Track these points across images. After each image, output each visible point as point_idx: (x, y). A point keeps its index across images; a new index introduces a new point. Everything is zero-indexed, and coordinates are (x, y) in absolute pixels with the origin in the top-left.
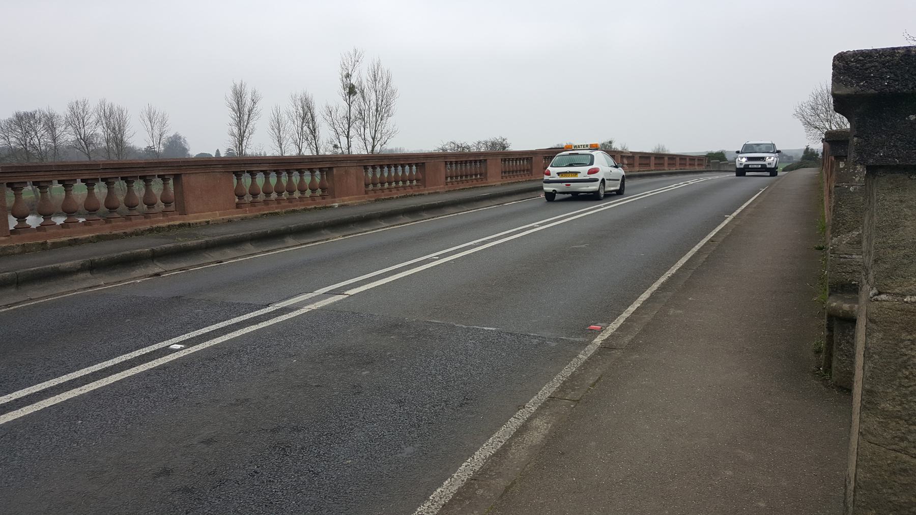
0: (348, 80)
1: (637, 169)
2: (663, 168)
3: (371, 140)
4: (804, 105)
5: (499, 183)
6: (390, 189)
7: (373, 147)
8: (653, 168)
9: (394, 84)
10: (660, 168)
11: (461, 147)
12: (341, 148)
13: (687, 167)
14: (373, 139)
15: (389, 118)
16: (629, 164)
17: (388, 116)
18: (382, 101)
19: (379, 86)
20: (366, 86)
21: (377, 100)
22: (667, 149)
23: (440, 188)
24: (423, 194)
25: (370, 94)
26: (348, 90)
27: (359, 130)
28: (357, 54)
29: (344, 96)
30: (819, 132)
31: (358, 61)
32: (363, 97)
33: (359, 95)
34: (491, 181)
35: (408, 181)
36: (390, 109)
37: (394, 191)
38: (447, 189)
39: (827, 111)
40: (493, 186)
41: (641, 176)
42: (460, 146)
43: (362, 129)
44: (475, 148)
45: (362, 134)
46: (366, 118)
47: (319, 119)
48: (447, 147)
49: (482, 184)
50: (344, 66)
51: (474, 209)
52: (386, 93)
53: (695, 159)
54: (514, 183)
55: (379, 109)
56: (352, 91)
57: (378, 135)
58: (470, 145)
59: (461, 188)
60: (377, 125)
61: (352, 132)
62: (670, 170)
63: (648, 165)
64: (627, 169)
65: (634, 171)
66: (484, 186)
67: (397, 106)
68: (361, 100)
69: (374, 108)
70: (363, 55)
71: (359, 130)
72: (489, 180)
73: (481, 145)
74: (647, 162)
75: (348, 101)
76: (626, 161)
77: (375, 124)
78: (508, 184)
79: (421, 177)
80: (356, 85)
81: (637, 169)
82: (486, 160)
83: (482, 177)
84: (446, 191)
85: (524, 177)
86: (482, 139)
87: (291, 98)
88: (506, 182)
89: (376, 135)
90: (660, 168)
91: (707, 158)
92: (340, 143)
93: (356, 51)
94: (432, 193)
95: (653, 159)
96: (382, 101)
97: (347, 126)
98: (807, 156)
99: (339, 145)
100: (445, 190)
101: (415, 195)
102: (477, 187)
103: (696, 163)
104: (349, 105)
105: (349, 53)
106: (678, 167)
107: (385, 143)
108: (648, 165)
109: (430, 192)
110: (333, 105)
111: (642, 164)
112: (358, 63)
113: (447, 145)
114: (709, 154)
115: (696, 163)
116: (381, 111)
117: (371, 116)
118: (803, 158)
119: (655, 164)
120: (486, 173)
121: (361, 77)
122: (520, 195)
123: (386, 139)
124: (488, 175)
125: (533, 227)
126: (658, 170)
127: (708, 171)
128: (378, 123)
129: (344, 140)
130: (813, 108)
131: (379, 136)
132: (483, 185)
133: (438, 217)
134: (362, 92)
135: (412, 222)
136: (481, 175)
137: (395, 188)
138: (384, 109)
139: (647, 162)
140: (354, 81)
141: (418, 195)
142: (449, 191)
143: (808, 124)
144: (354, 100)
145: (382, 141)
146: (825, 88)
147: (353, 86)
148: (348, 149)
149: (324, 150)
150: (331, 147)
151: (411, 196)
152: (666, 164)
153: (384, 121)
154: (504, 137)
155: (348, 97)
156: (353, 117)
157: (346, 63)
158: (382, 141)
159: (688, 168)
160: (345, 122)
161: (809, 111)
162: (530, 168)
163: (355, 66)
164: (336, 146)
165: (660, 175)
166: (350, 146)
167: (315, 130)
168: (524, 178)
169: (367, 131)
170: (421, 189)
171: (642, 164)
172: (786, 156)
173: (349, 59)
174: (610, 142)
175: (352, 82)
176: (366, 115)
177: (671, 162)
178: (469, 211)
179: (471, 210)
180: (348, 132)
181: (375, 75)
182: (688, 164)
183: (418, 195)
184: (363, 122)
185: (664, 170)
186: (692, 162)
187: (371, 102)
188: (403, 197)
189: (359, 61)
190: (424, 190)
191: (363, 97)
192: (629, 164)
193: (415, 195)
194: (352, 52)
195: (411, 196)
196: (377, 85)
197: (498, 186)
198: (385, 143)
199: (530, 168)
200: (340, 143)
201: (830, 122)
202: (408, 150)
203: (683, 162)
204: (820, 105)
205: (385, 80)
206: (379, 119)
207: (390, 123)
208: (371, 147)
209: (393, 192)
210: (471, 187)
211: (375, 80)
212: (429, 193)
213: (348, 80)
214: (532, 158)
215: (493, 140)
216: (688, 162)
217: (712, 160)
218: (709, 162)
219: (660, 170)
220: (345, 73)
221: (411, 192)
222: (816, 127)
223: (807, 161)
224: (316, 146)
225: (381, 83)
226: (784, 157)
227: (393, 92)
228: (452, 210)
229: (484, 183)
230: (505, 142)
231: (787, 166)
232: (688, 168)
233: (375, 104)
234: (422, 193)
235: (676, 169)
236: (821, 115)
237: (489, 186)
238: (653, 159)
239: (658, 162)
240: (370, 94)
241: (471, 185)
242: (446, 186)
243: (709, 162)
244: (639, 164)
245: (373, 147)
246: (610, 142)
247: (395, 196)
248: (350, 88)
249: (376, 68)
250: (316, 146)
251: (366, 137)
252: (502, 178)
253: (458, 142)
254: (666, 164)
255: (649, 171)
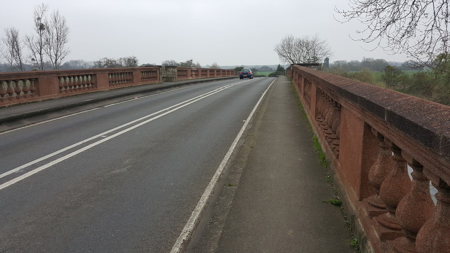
0: (39, 21)
1: (200, 77)
2: (214, 76)
3: (55, 56)
4: (278, 45)
5: (107, 89)
6: (66, 91)
7: (56, 60)
8: (209, 77)
9: (67, 24)
10: (213, 76)
11: (111, 61)
12: (37, 60)
13: (226, 76)
14: (56, 55)
15: (65, 44)
16: (196, 75)
17: (64, 42)
18: (60, 34)
19: (58, 26)
20: (50, 25)
21: (57, 33)
22: (218, 64)
23: (54, 96)
24: (37, 102)
25: (53, 30)
26: (39, 27)
27: (47, 50)
28: (44, 7)
29: (37, 30)
30: (285, 58)
31: (45, 11)
32: (49, 31)
33: (46, 30)
34: (100, 88)
35: (78, 86)
36: (65, 38)
37: (83, 90)
38: (61, 96)
39: (289, 48)
40: (102, 91)
41: (202, 82)
42: (110, 60)
43: (49, 50)
44: (118, 61)
45: (49, 52)
46: (51, 43)
47: (21, 45)
48: (102, 60)
49: (93, 90)
50: (36, 13)
51: (76, 113)
52: (62, 30)
53: (229, 71)
54: (119, 89)
55: (59, 38)
56: (42, 27)
57: (59, 53)
58: (116, 60)
59: (74, 94)
60: (58, 48)
61: (43, 51)
62: (217, 77)
63: (206, 75)
64: (194, 78)
65: (199, 79)
66: (95, 92)
67: (69, 37)
68: (47, 33)
69: (56, 38)
70: (48, 7)
71: (47, 50)
72: (99, 88)
73: (122, 60)
74: (206, 73)
75: (40, 33)
76: (194, 73)
77: (56, 47)
78: (115, 89)
79: (34, 88)
80: (44, 24)
81: (200, 77)
82: (95, 75)
83: (93, 86)
84: (60, 98)
85: (127, 84)
86: (123, 57)
87: (5, 31)
88: (113, 88)
89: (58, 53)
90: (213, 76)
91: (235, 71)
92: (36, 57)
93: (43, 4)
94: (46, 100)
95: (208, 71)
96: (60, 34)
97: (39, 48)
98: (279, 69)
99: (35, 59)
100: (60, 97)
101: (28, 103)
102: (89, 93)
103: (230, 73)
104: (40, 35)
105: (39, 6)
106: (222, 76)
107: (63, 58)
108: (206, 75)
109: (45, 99)
110: (30, 36)
111: (203, 75)
112: (45, 12)
113: (102, 59)
114: (236, 68)
115: (230, 73)
116: (60, 40)
117: (54, 41)
118: (277, 70)
119: (210, 74)
120: (96, 83)
121: (47, 19)
122: (119, 98)
123: (64, 55)
124: (98, 84)
125: (200, 97)
126: (211, 78)
127: (236, 77)
128: (59, 46)
129: (38, 56)
130: (282, 47)
131: (59, 54)
132: (94, 91)
133: (38, 122)
134: (48, 28)
135: (8, 130)
136: (92, 84)
137: (74, 89)
138: (62, 39)
139: (206, 73)
140: (43, 22)
141: (32, 102)
142: (63, 97)
143: (280, 54)
144: (43, 33)
145: (62, 56)
146: (288, 37)
147: (43, 25)
148: (41, 61)
149: (25, 62)
150: (30, 60)
151: (25, 104)
152: (215, 74)
153: (62, 45)
154: (134, 56)
155: (39, 31)
156: (43, 43)
157: (37, 11)
158: (62, 56)
159: (227, 76)
160: (38, 45)
161: (280, 48)
162: (156, 76)
163: (43, 13)
164: (33, 59)
165: (212, 80)
166: (42, 60)
167: (18, 50)
168: (127, 85)
169: (52, 51)
170: (35, 97)
171: (203, 75)
172: (269, 68)
173: (40, 9)
174: (191, 61)
175: (41, 22)
176: (51, 42)
177: (218, 73)
178: (71, 114)
179: (74, 113)
180: (41, 51)
181: (55, 19)
182: (226, 74)
183: (32, 102)
184: (49, 46)
185: (214, 77)
186: (229, 73)
187: (54, 34)
188: (18, 105)
189: (46, 10)
190: (39, 98)
191: (49, 31)
192: (196, 75)
193: (28, 103)
194: (41, 5)
195: (25, 104)
196: (57, 25)
197: (107, 91)
198: (63, 58)
199: (131, 78)
200: (36, 57)
201: (290, 54)
202: (86, 61)
203: (224, 73)
204: (286, 45)
205: (62, 22)
206: (59, 44)
207: (65, 47)
208: (55, 60)
209: (5, 102)
210: (84, 93)
211: (56, 22)
212: (43, 101)
213: (39, 21)
214: (132, 72)
215: (128, 57)
216: (226, 73)
217: (238, 71)
218: (236, 72)
219: (213, 77)
220: (37, 17)
221: (25, 100)
222: (284, 56)
223: (279, 71)
224: (20, 60)
225: (59, 24)
226: (269, 69)
227: (67, 29)
228: (55, 115)
229: (95, 90)
230: (135, 59)
231: (271, 74)
232: (227, 76)
233: (56, 35)
234: (37, 100)
235: (221, 77)
236: (286, 50)
237: (99, 92)
238: (208, 71)
239: (211, 73)
240: (53, 30)
241: (83, 92)
242: (60, 94)
243: (236, 72)
244: (201, 75)
245: (56, 60)
246: (191, 61)
247: (7, 105)
248: (40, 26)
249: (56, 15)
250: (20, 60)
251: (51, 54)
252: (110, 86)
253: (109, 58)
254: (215, 74)
255: (207, 78)
